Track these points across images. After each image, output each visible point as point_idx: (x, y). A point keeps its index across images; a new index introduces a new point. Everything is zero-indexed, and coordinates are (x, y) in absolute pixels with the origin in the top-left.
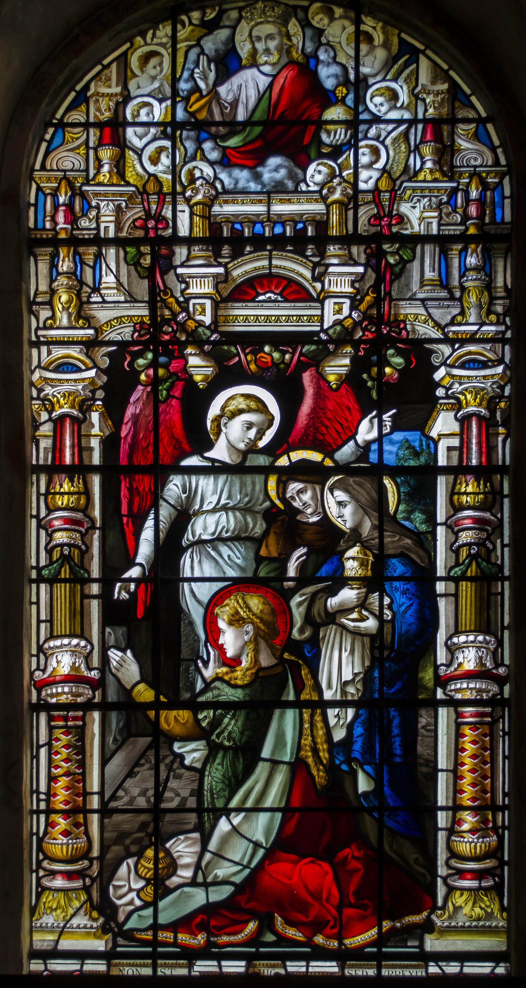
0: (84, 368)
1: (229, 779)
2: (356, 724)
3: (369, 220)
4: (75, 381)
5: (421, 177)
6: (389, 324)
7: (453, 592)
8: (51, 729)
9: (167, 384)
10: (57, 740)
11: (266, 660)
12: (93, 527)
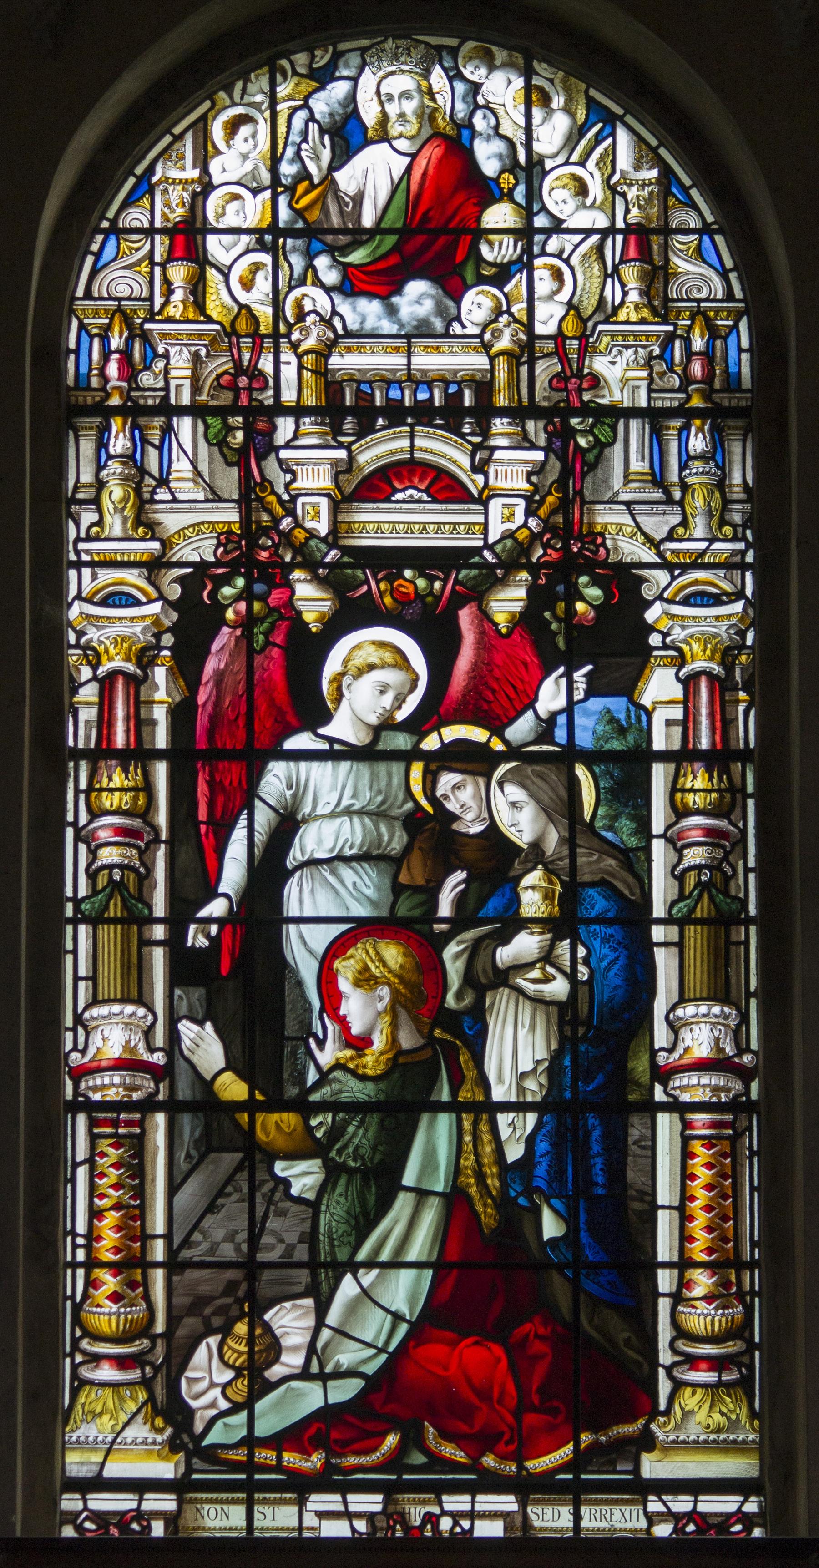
0: (144, 599)
1: (356, 1218)
2: (540, 1137)
3: (550, 381)
4: (132, 619)
5: (622, 316)
6: (580, 538)
7: (676, 939)
8: (94, 1139)
9: (265, 625)
10: (103, 1155)
11: (407, 1040)
12: (157, 840)
